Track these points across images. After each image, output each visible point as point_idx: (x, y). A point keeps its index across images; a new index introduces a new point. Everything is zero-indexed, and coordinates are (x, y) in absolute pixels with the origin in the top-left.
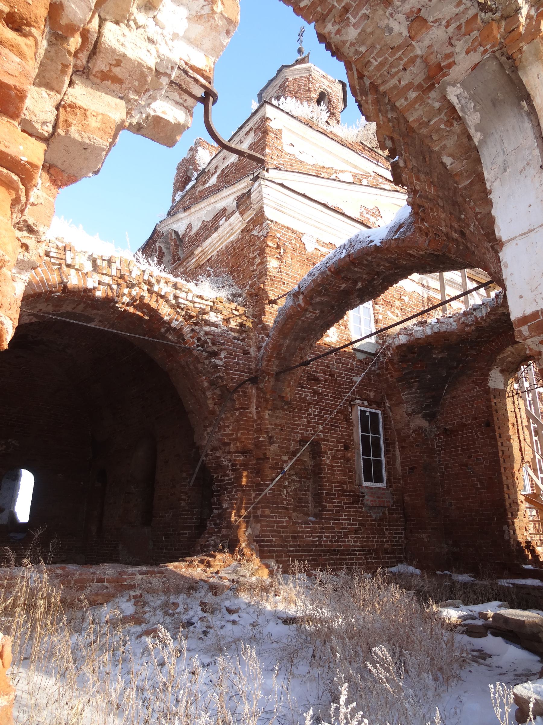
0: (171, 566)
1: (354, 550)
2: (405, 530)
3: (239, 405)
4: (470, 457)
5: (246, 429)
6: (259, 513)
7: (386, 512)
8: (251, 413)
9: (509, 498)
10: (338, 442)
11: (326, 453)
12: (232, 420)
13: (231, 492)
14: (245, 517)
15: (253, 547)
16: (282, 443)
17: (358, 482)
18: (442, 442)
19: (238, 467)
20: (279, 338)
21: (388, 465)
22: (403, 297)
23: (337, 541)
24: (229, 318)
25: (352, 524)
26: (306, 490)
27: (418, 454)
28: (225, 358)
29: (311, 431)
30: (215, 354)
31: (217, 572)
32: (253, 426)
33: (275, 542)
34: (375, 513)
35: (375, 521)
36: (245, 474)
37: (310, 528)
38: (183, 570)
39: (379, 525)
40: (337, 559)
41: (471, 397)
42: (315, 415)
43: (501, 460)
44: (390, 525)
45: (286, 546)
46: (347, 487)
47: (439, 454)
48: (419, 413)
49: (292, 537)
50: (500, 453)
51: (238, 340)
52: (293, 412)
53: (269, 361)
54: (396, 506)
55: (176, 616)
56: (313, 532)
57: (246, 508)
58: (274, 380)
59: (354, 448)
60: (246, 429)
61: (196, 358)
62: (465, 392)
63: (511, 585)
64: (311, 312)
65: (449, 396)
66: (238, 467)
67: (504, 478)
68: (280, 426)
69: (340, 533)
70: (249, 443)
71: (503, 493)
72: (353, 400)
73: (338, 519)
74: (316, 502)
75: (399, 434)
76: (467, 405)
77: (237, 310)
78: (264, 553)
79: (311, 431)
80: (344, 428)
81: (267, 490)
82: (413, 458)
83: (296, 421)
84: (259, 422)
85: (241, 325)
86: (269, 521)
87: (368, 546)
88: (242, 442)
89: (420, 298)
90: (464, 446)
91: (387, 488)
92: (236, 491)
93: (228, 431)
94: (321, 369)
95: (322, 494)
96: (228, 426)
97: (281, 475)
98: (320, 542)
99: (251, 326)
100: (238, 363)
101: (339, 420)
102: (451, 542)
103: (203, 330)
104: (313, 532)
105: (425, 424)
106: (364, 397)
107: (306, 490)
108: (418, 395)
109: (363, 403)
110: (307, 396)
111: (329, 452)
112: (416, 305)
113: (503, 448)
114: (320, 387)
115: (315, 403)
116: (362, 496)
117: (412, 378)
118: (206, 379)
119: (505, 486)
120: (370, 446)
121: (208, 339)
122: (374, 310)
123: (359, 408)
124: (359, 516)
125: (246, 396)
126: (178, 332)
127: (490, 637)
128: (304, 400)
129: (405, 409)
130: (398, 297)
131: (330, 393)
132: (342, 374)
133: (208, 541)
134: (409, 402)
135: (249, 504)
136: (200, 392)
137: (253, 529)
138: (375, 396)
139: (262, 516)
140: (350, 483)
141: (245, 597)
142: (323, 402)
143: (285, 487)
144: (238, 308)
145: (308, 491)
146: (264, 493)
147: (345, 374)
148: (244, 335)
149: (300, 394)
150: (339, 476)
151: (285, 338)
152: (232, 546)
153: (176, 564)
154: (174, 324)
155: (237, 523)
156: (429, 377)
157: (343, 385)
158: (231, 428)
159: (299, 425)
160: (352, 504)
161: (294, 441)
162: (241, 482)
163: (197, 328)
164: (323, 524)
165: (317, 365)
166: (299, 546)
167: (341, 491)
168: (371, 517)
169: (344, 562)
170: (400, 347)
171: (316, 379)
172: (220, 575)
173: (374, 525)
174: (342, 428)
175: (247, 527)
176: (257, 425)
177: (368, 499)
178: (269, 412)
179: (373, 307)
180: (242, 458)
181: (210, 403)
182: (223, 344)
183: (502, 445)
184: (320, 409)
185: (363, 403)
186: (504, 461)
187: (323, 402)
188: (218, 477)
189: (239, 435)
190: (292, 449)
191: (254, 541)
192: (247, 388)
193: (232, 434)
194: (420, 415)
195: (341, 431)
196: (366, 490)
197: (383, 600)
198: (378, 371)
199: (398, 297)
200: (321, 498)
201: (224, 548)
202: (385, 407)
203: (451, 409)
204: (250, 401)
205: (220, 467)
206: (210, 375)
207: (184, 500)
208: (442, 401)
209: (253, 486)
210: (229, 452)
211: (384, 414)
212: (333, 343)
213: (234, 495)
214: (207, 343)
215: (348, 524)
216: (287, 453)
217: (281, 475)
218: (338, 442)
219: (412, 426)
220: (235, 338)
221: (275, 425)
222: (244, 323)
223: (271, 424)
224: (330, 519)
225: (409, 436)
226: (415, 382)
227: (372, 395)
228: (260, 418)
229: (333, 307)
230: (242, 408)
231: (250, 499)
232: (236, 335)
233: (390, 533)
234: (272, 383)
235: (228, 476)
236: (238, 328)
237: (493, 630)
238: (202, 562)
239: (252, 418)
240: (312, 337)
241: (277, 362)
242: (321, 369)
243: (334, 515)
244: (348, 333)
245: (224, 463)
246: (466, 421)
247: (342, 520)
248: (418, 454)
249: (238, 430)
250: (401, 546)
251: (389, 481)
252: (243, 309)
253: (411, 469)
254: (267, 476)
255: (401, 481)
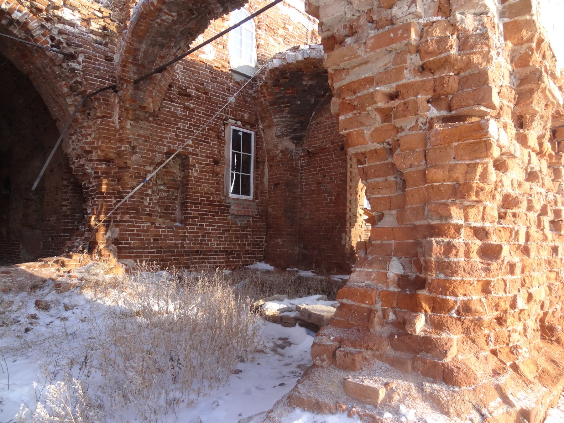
0: (23, 266)
1: (217, 252)
2: (266, 235)
3: (101, 113)
4: (325, 176)
5: (107, 138)
6: (118, 218)
7: (251, 220)
8: (113, 122)
9: (350, 211)
10: (207, 157)
11: (194, 166)
12: (94, 128)
13: (93, 198)
14: (105, 222)
15: (111, 248)
16: (146, 154)
17: (225, 194)
18: (304, 163)
19: (100, 174)
20: (133, 40)
21: (257, 180)
22: (287, 26)
23: (201, 244)
24: (90, 19)
25: (216, 230)
26: (174, 199)
27: (282, 172)
28: (83, 62)
29: (179, 144)
30: (72, 57)
31: (69, 272)
32: (115, 136)
33: (133, 244)
34: (239, 221)
35: (240, 227)
36: (105, 181)
37: (173, 232)
38: (36, 269)
39: (243, 231)
40: (199, 259)
41: (333, 123)
42: (184, 130)
43: (349, 179)
44: (253, 231)
45: (147, 248)
46: (214, 198)
47: (301, 173)
48: (287, 136)
49: (154, 240)
50: (349, 174)
51: (101, 44)
52: (160, 125)
53: (125, 66)
54: (260, 215)
55: (7, 313)
56: (176, 236)
57: (106, 214)
58: (132, 88)
59: (224, 164)
60: (107, 138)
61: (51, 60)
62: (328, 119)
63: (340, 280)
64: (166, 13)
65: (315, 122)
66: (100, 174)
67: (348, 195)
68: (144, 137)
69: (205, 237)
70: (111, 152)
71: (345, 206)
72: (226, 119)
73: (203, 225)
74: (183, 210)
75: (269, 154)
76: (328, 131)
77: (100, 11)
78: (121, 255)
79: (179, 144)
80: (215, 144)
81: (127, 197)
82: (278, 176)
83: (163, 133)
84: (121, 132)
85: (104, 28)
86: (128, 226)
87: (230, 248)
88: (103, 151)
89: (305, 30)
90: (321, 166)
91: (253, 200)
92: (98, 198)
93: (90, 139)
94: (194, 86)
95: (187, 203)
96: (90, 135)
97: (142, 184)
98: (182, 244)
99: (115, 30)
100: (99, 69)
101: (211, 136)
102: (302, 246)
103: (55, 28)
104: (176, 236)
105: (291, 146)
106: (238, 117)
107: (174, 199)
108: (287, 119)
109: (236, 123)
110: (177, 110)
111: (197, 165)
112: (300, 37)
113: (352, 170)
114: (192, 103)
115: (185, 118)
116: (228, 207)
117: (283, 103)
118: (65, 84)
119: (348, 201)
120: (242, 165)
121: (61, 38)
122: (257, 34)
123: (232, 127)
124: (224, 223)
125: (107, 102)
126: (24, 26)
127: (297, 327)
128: (174, 115)
129: (276, 131)
130: (283, 25)
131: (202, 110)
132: (217, 93)
133: (74, 242)
134: (279, 125)
135: (109, 209)
136: (61, 99)
137: (112, 233)
138: (249, 117)
139: (121, 221)
140: (216, 194)
141: (88, 294)
142: (194, 118)
143: (147, 195)
144: (102, 9)
145: (176, 200)
146: (123, 200)
147: (219, 93)
148: (107, 40)
149: (169, 108)
150: (206, 187)
151: (140, 42)
152: (91, 247)
153: (28, 264)
154: (16, 15)
155: (96, 227)
156: (299, 103)
157: (217, 104)
158: (93, 136)
159: (166, 138)
160: (218, 212)
161: (159, 153)
162: (101, 189)
163: (48, 25)
164: (187, 229)
165: (190, 81)
166: (161, 248)
167: (207, 201)
168: (236, 224)
169: (206, 261)
170: (273, 71)
171: (189, 95)
172: (71, 274)
173: (239, 231)
174: (213, 144)
175: (106, 231)
176: (119, 134)
177: (234, 209)
178: (132, 122)
179: (256, 31)
180: (104, 166)
181: (71, 110)
182: (80, 46)
183: (351, 167)
184: (190, 124)
185: (236, 123)
186: (351, 181)
187: (194, 118)
188: (85, 184)
189: (100, 143)
190: (157, 160)
191: (113, 243)
192: (110, 97)
193: (94, 143)
194: (288, 138)
195: (211, 147)
196: (233, 201)
197: (213, 297)
198: (254, 95)
199: (283, 25)
200: (187, 206)
201: (84, 249)
202: (258, 128)
203: (315, 134)
204: (112, 110)
205: (85, 174)
206: (69, 80)
207: (66, 206)
208: (308, 126)
209: (114, 194)
210: (91, 160)
211: (257, 134)
212: (208, 61)
213: (95, 201)
214: (62, 43)
215: (212, 230)
216: (151, 164)
217: (142, 184)
218: (207, 157)
219: (280, 147)
220: (96, 42)
221: (138, 136)
222: (107, 26)
223: (134, 135)
224: (194, 225)
225: (276, 156)
226: (286, 106)
227: (246, 116)
228: (122, 128)
229: (191, 10)
230: (104, 117)
231: (111, 205)
232: (98, 38)
233: (252, 238)
234: (131, 92)
235: (91, 183)
236: (100, 31)
237: (300, 322)
238: (57, 262)
239: (115, 127)
240: (173, 44)
241: (134, 69)
242: (194, 86)
243: (198, 221)
244: (227, 53)
245: (89, 171)
246: (326, 145)
247: (206, 226)
248: (282, 172)
249: (99, 138)
250: (262, 248)
251: (255, 194)
252: (109, 11)
253: (276, 184)
254: (128, 184)
255: (267, 195)
